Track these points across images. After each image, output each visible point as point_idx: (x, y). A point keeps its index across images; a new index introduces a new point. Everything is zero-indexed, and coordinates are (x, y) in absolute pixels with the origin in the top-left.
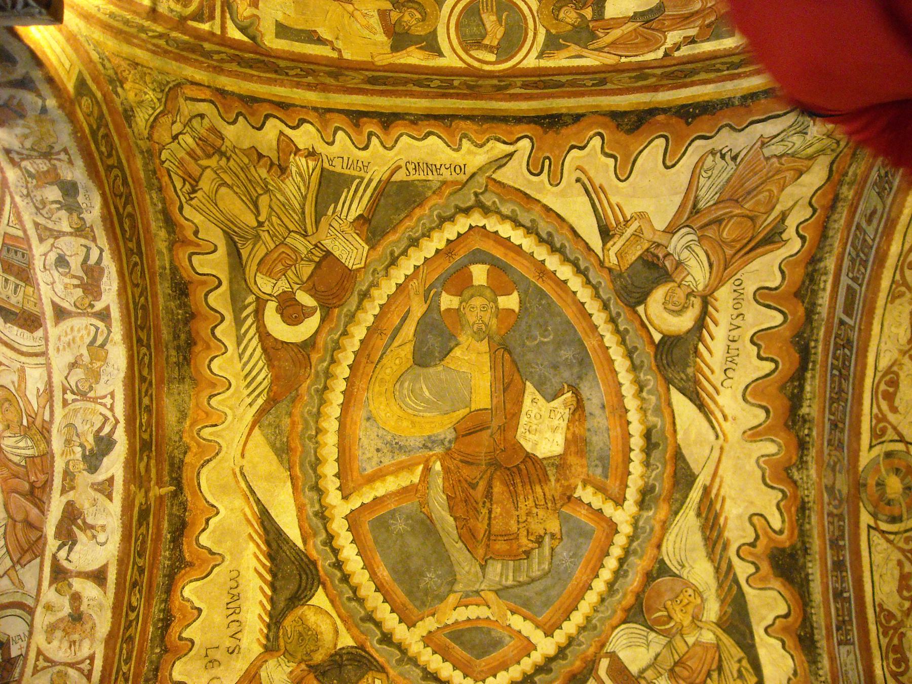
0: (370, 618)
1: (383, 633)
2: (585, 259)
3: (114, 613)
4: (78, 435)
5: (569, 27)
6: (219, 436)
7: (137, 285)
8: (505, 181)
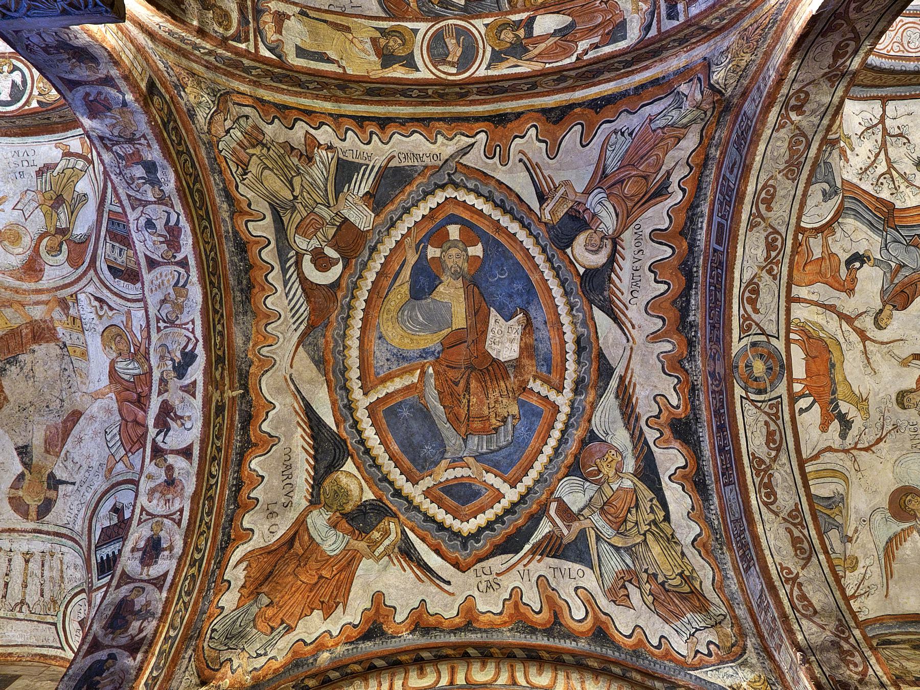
0: (385, 479)
1: (394, 489)
2: (527, 217)
3: (197, 478)
4: (169, 352)
5: (508, 45)
6: (274, 353)
7: (208, 243)
8: (469, 164)
